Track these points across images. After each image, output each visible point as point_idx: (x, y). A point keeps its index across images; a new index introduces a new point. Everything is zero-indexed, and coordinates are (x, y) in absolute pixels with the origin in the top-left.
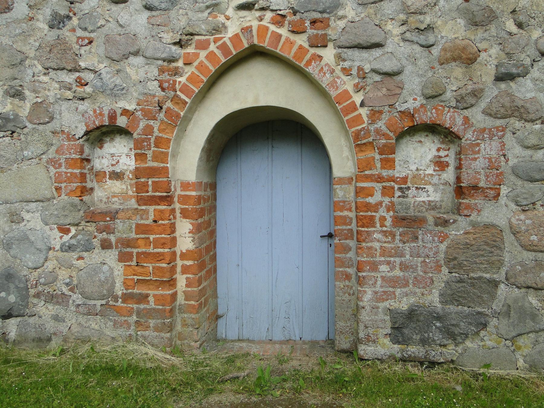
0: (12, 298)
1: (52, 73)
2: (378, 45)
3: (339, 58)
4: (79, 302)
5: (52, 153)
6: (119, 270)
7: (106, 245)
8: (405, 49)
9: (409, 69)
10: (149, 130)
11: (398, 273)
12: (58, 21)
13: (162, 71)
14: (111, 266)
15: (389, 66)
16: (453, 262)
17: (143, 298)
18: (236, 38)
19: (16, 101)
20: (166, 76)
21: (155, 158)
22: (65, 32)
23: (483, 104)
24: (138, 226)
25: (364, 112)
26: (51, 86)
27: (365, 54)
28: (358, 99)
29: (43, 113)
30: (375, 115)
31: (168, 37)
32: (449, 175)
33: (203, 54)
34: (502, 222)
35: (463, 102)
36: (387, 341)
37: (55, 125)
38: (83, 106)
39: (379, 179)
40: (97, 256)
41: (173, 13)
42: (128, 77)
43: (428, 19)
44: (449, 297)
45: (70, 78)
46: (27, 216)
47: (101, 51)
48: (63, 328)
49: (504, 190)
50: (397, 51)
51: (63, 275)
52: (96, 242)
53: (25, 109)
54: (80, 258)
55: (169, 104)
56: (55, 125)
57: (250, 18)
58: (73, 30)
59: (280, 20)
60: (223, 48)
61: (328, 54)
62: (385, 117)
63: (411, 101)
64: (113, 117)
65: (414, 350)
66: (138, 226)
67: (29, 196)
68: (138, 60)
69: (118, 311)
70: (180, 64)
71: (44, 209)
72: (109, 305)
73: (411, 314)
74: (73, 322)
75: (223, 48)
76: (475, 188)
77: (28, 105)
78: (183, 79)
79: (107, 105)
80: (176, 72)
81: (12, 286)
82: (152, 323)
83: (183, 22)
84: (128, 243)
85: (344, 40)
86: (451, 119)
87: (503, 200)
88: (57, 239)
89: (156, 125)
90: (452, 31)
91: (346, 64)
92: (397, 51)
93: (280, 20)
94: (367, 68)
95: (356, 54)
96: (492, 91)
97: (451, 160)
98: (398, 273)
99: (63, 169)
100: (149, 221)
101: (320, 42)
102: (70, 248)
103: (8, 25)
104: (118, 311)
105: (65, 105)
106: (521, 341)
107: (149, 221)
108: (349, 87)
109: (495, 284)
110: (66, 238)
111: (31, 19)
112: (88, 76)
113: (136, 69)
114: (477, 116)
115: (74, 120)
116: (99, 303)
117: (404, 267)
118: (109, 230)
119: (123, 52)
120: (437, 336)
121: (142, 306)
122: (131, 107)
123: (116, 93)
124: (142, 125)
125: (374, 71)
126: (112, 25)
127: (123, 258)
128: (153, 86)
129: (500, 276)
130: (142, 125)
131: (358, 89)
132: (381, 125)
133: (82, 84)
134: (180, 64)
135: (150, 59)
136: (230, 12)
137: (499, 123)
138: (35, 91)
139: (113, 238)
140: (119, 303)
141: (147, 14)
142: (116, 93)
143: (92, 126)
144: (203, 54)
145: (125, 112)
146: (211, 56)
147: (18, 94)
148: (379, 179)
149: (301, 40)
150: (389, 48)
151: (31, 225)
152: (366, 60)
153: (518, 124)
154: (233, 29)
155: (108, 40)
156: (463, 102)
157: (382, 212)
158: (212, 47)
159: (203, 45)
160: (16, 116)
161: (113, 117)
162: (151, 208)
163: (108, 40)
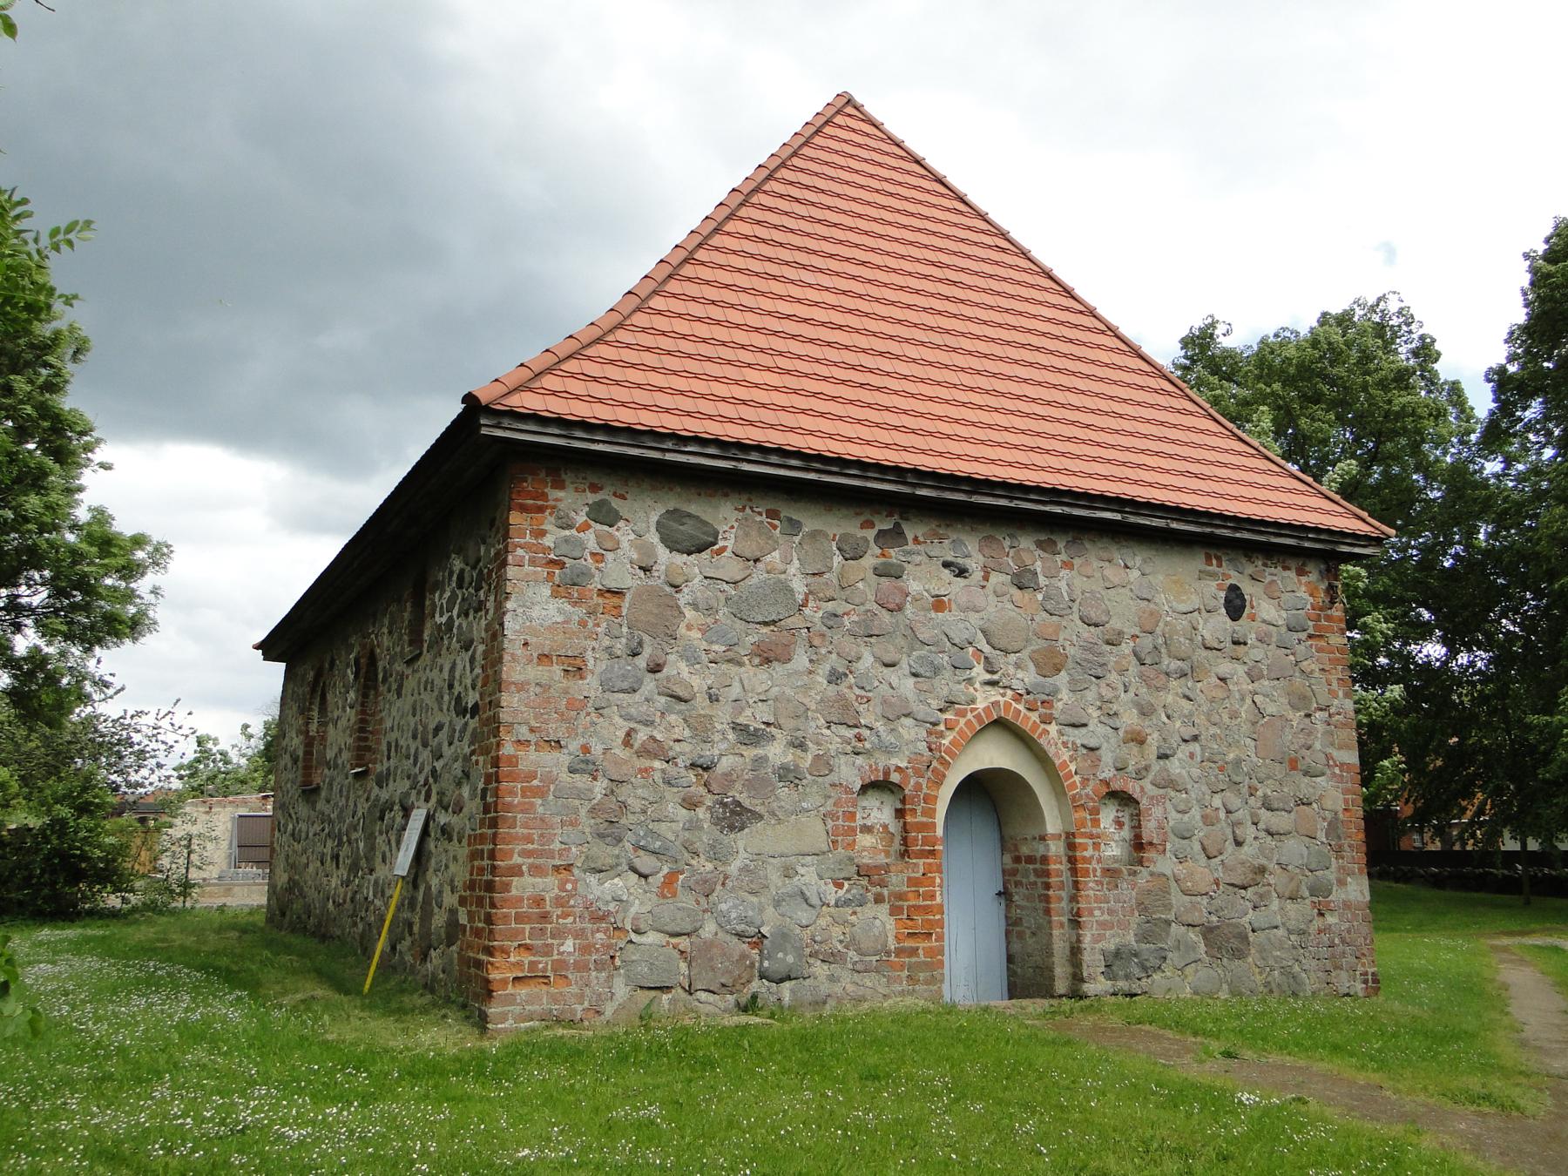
0: (790, 959)
1: (833, 727)
2: (1085, 725)
3: (1061, 733)
4: (856, 959)
5: (829, 806)
6: (890, 924)
7: (879, 899)
8: (1101, 729)
9: (1105, 746)
10: (918, 787)
11: (1106, 917)
12: (835, 677)
13: (929, 733)
14: (881, 923)
15: (1092, 743)
16: (1142, 908)
17: (913, 952)
18: (986, 709)
19: (799, 752)
20: (933, 739)
21: (924, 813)
22: (843, 688)
23: (1150, 777)
24: (909, 878)
25: (1077, 779)
26: (836, 738)
27: (1076, 731)
28: (1073, 767)
29: (823, 764)
30: (1085, 781)
31: (935, 704)
32: (1126, 833)
33: (962, 721)
34: (1168, 873)
35: (1140, 775)
36: (1102, 978)
37: (833, 778)
38: (860, 760)
39: (1091, 836)
40: (870, 910)
41: (936, 681)
42: (901, 736)
43: (1115, 707)
44: (1144, 937)
45: (849, 733)
46: (801, 870)
47: (879, 710)
48: (838, 989)
49: (1168, 846)
50: (1096, 732)
51: (836, 931)
52: (870, 896)
53: (806, 761)
54: (855, 913)
55: (935, 763)
56: (833, 778)
57: (994, 695)
58: (850, 687)
59: (1018, 697)
60: (978, 717)
61: (1053, 729)
62: (1091, 783)
63: (1107, 773)
64: (887, 773)
65: (1122, 984)
66: (909, 878)
67: (806, 850)
68: (908, 722)
69: (892, 966)
70: (942, 727)
71: (820, 863)
72: (883, 961)
73: (1117, 954)
74: (847, 983)
75: (978, 717)
76: (1151, 844)
77: (810, 757)
78: (945, 742)
79: (882, 761)
80: (941, 735)
81: (789, 946)
82: (922, 976)
83: (945, 692)
84: (901, 896)
85: (1062, 719)
86: (1133, 788)
87: (1168, 854)
88: (832, 894)
89: (923, 781)
90: (1129, 719)
91: (1065, 738)
92: (1096, 732)
93: (1018, 697)
94: (1079, 742)
95: (1070, 730)
96: (1156, 766)
97: (1126, 820)
98: (1106, 917)
99: (840, 822)
100: (919, 875)
101: (1047, 720)
102: (847, 903)
103: (789, 675)
104: (892, 966)
105: (843, 759)
106: (1188, 970)
107: (919, 875)
108: (1066, 757)
109: (1168, 923)
110: (841, 893)
111: (811, 672)
112: (866, 733)
113: (909, 730)
114: (1146, 783)
115: (851, 773)
116: (874, 958)
117: (1111, 912)
118: (882, 884)
119: (896, 713)
120: (1137, 971)
121: (914, 960)
122: (903, 765)
123: (889, 750)
124: (912, 782)
125: (1083, 746)
126: (885, 687)
127: (895, 911)
128: (922, 746)
129: (1171, 917)
130: (912, 782)
131: (1072, 759)
132: (1089, 790)
133: (859, 738)
134: (942, 727)
135: (920, 721)
136: (977, 685)
137: (1162, 791)
138: (818, 744)
139: (885, 892)
140: (893, 958)
141: (912, 680)
142: (889, 750)
143: (867, 781)
144: (962, 721)
145: (898, 769)
146: (968, 723)
147: (801, 746)
148: (1091, 836)
149: (1034, 716)
150: (1091, 727)
151: (806, 879)
152: (1079, 737)
153: (1173, 794)
154: (980, 705)
155: (885, 702)
156: (1140, 775)
157: (1094, 864)
158: (969, 716)
159: (962, 714)
160: (797, 766)
161: (887, 773)
162: (921, 861)
163: (885, 702)
